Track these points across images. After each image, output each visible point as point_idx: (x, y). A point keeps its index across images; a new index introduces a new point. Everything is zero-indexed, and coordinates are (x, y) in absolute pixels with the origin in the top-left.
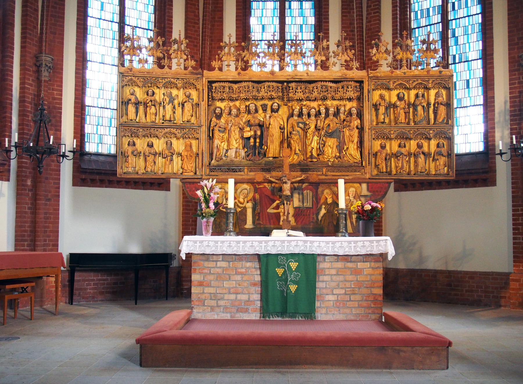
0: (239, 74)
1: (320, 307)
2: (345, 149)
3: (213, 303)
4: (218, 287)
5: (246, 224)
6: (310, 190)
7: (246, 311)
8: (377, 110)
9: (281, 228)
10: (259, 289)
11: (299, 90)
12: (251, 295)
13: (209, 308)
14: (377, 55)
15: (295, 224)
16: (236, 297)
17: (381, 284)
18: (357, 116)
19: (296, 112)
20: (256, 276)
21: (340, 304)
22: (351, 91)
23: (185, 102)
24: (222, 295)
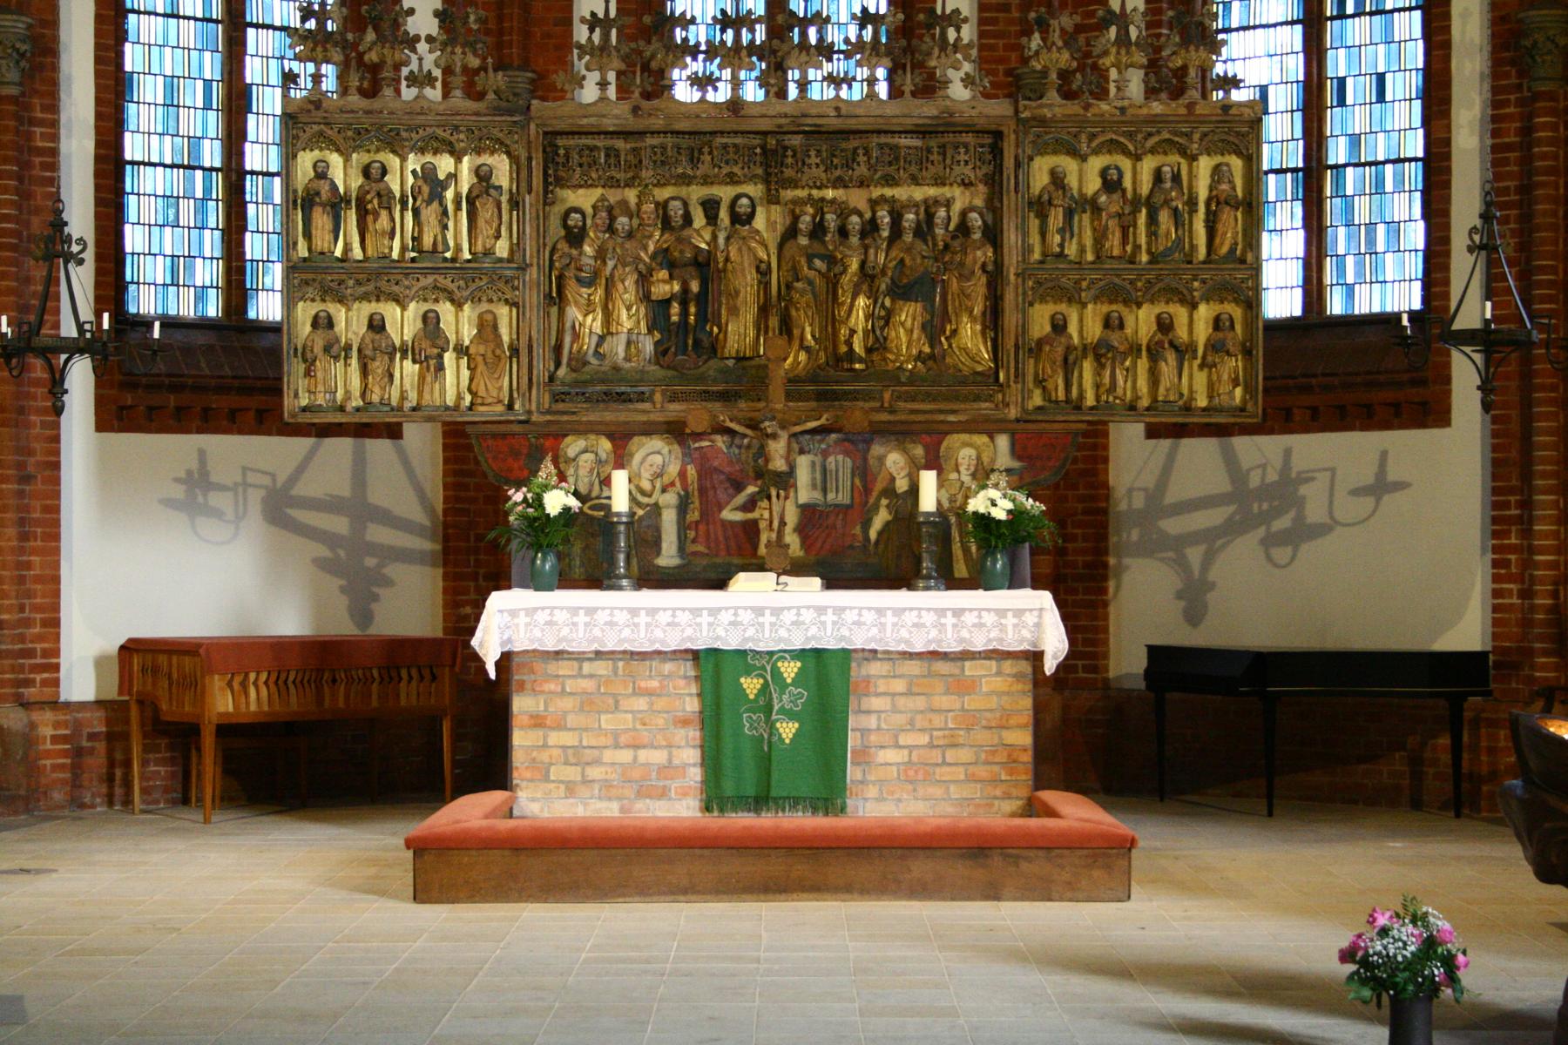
0: (635, 110)
1: (862, 782)
2: (948, 333)
3: (572, 773)
4: (586, 730)
5: (658, 553)
6: (847, 453)
7: (663, 794)
8: (1043, 217)
9: (761, 568)
10: (694, 734)
11: (814, 160)
12: (675, 752)
13: (562, 787)
14: (1044, 56)
15: (801, 554)
16: (635, 758)
17: (1027, 716)
20: (688, 699)
21: (915, 774)
22: (966, 163)
23: (478, 197)
24: (596, 752)
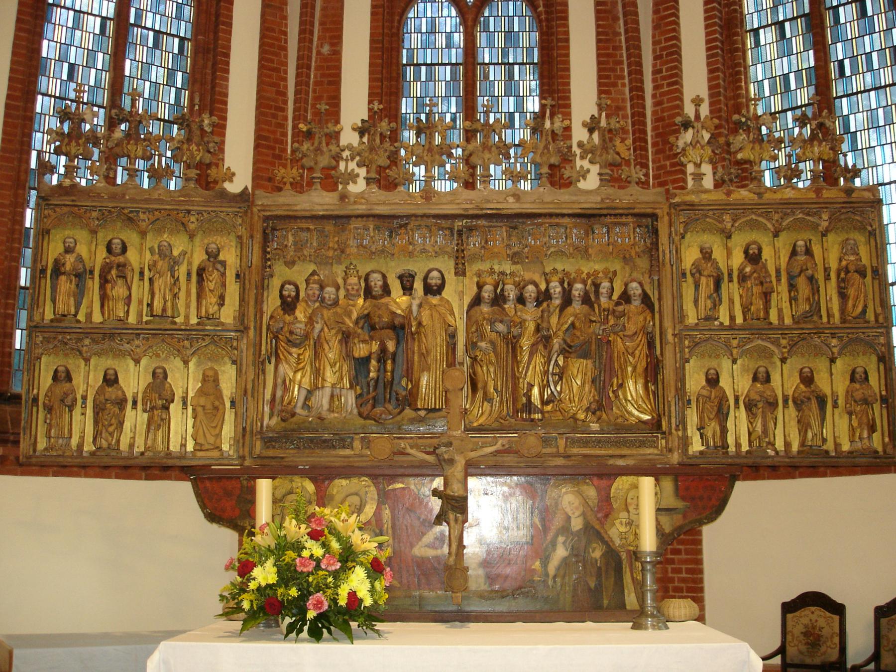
18: (643, 302)
19: (488, 292)
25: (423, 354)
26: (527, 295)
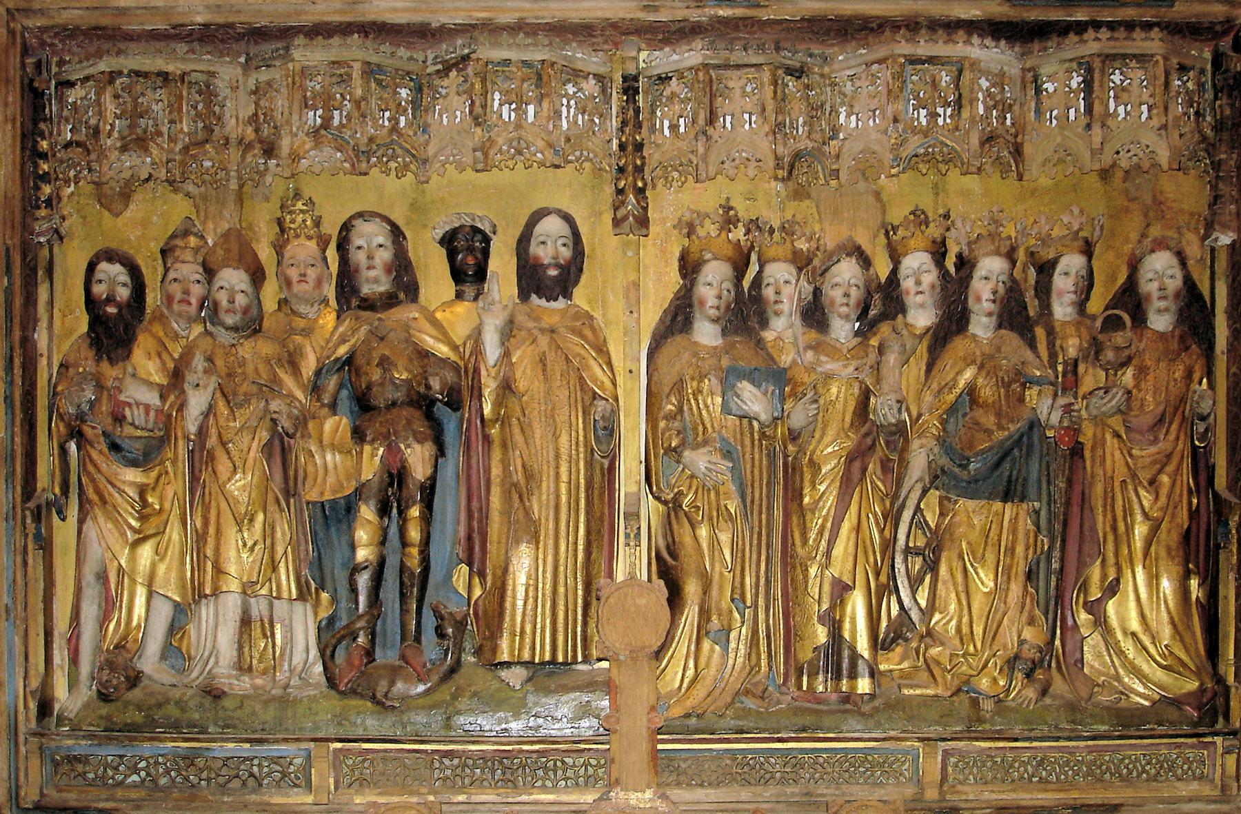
25: (515, 485)
26: (837, 294)
